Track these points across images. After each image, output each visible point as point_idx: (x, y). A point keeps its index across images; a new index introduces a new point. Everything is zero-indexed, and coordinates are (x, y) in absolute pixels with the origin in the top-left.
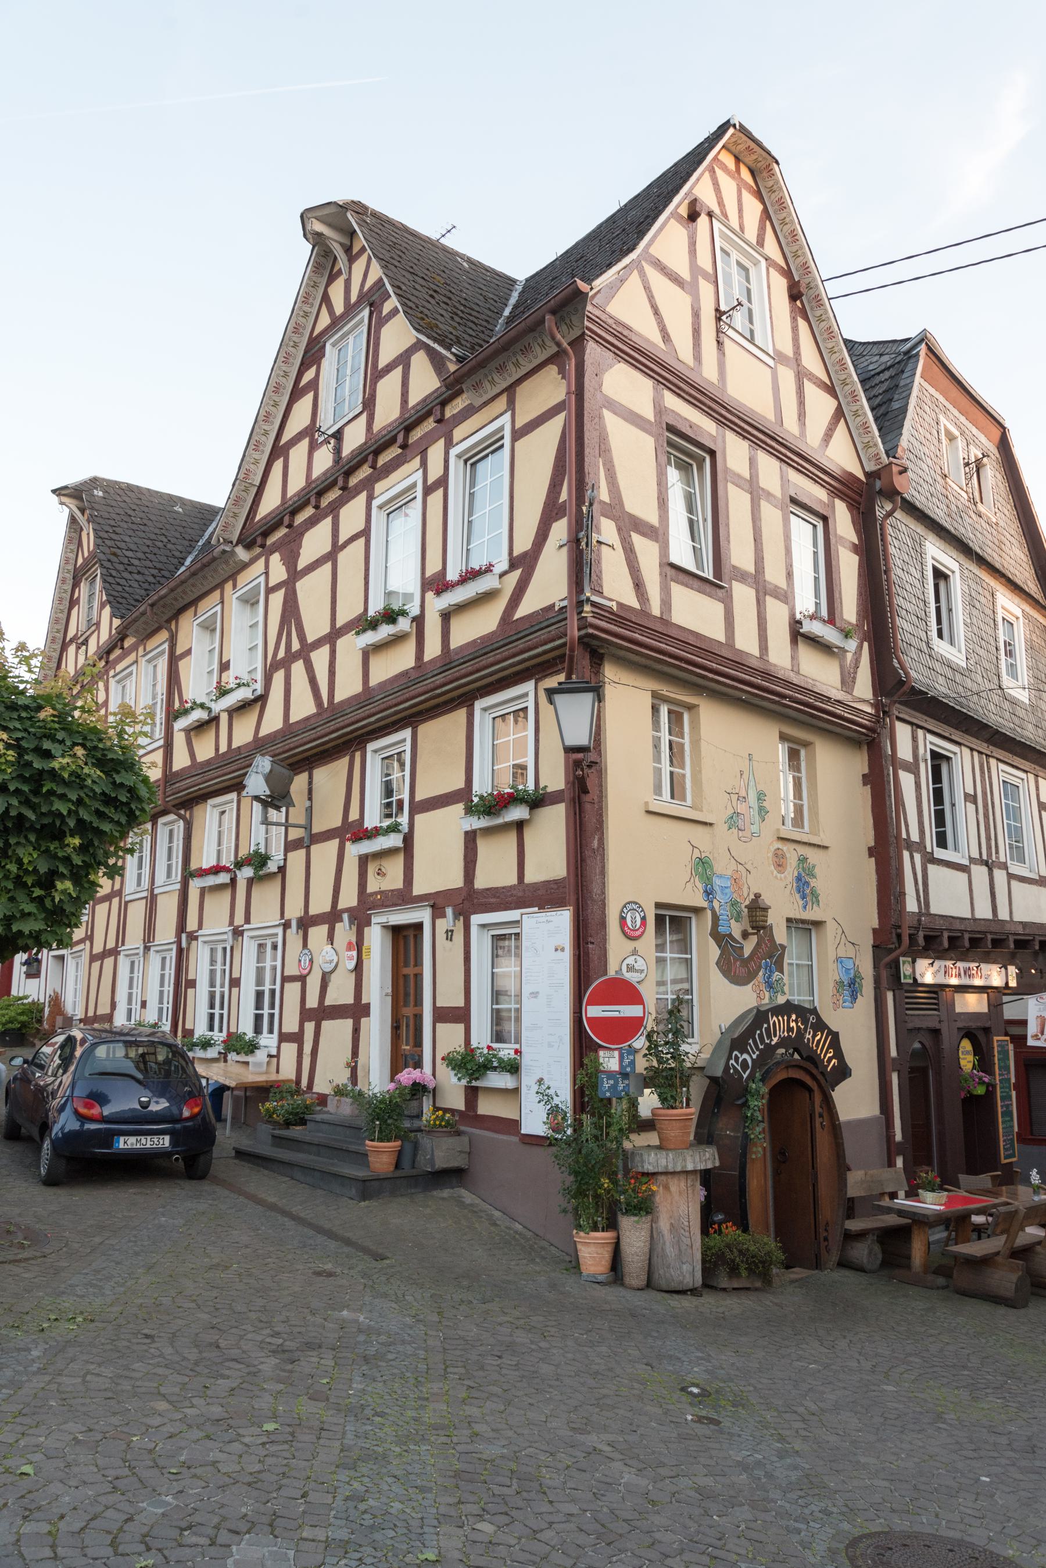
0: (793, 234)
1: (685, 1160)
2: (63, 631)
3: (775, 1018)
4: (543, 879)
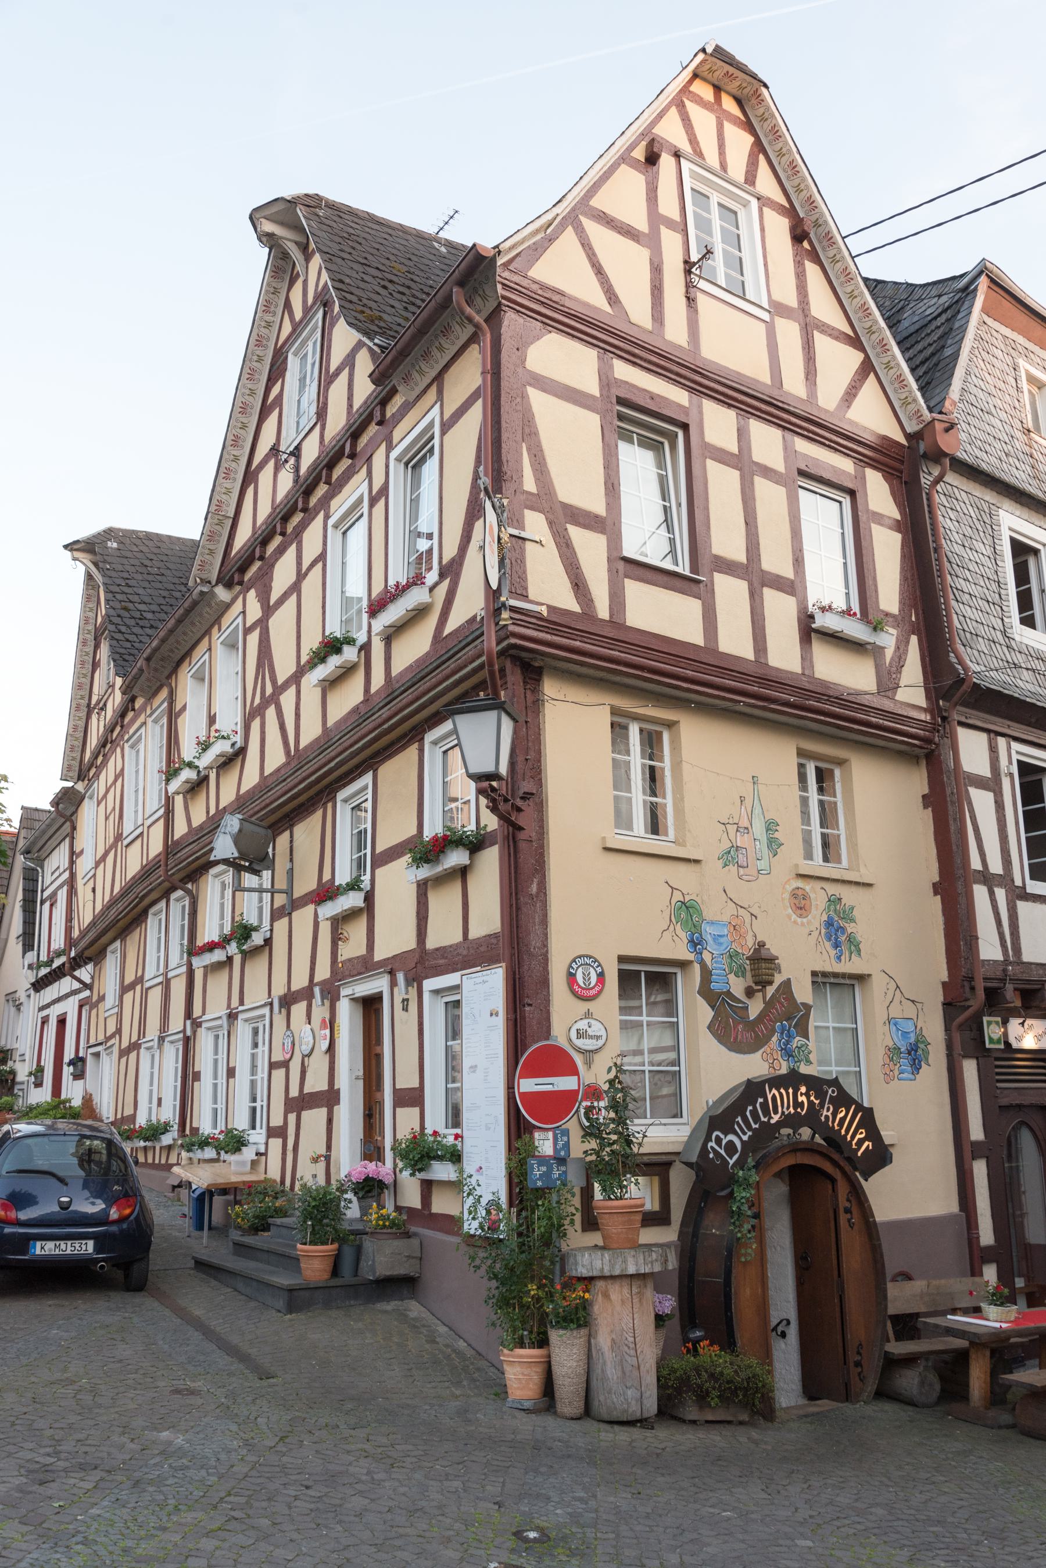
0: (793, 166)
1: (625, 1261)
2: (87, 697)
3: (774, 1091)
4: (483, 934)
